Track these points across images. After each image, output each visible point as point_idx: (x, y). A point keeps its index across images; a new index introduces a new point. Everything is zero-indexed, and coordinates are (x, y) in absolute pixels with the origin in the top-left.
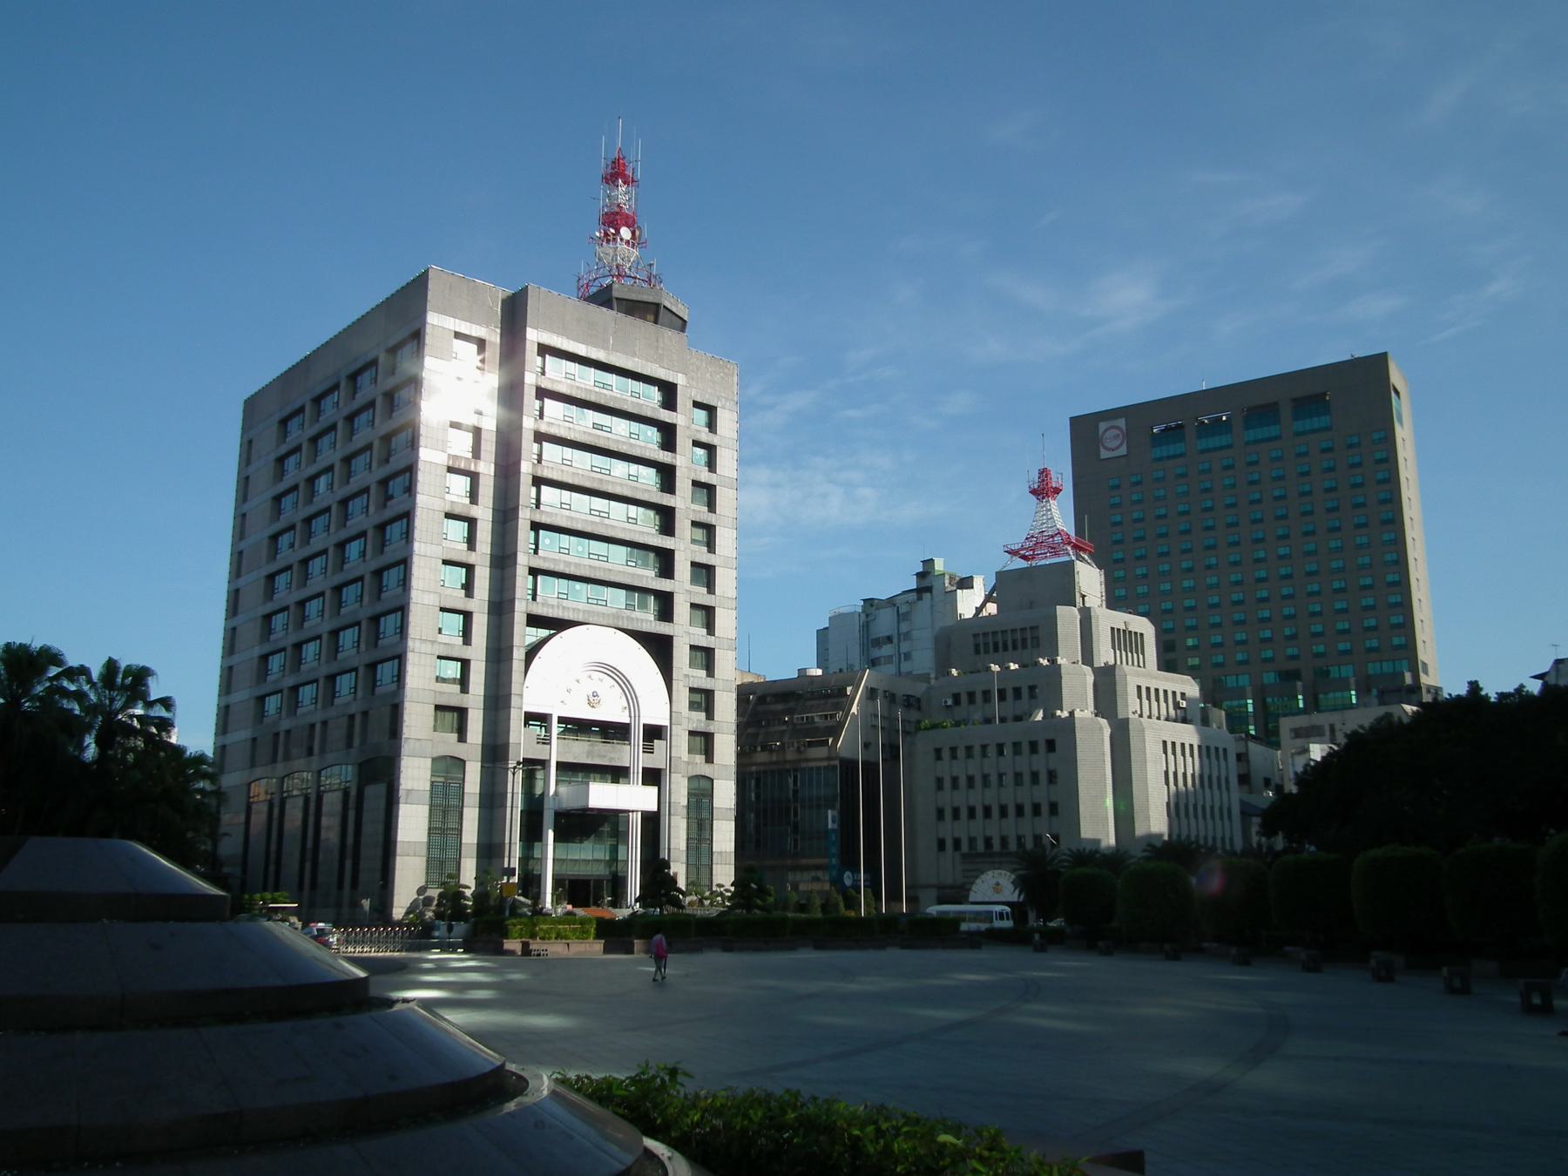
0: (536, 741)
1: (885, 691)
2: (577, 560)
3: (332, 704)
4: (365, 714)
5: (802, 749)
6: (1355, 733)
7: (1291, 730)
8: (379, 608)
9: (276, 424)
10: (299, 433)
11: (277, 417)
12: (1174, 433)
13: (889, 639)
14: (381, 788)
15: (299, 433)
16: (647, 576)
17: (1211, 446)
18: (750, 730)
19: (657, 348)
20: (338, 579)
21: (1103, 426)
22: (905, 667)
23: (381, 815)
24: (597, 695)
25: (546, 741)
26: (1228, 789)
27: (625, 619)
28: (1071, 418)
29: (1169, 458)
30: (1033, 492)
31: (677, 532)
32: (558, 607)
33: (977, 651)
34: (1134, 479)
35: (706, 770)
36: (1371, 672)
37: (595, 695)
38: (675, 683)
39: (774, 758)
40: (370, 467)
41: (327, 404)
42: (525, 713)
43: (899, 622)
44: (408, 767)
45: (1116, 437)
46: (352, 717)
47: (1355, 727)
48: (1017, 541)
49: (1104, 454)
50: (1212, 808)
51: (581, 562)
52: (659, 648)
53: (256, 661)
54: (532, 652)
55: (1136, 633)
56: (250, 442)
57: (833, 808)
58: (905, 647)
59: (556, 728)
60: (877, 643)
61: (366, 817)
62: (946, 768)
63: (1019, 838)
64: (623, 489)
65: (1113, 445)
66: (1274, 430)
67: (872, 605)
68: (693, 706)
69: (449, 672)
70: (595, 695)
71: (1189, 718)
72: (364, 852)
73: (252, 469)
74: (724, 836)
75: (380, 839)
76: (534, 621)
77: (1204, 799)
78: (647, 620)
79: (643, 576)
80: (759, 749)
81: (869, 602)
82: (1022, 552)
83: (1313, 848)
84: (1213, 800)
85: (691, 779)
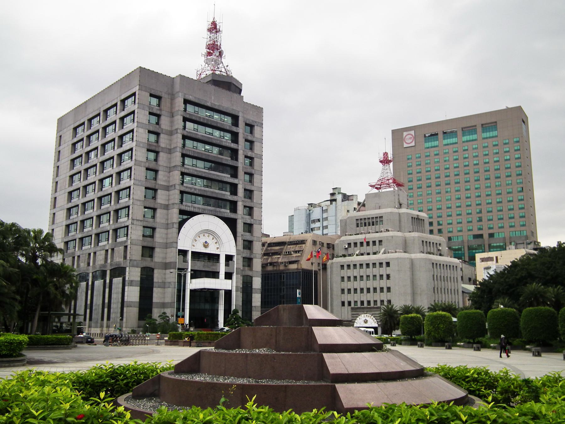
2: (199, 188)
3: (98, 245)
5: (287, 265)
6: (514, 261)
7: (480, 259)
8: (118, 207)
9: (72, 130)
10: (82, 133)
11: (73, 126)
13: (319, 220)
14: (120, 279)
15: (82, 133)
16: (227, 195)
17: (449, 143)
18: (265, 257)
19: (231, 101)
20: (101, 194)
21: (405, 134)
22: (325, 231)
23: (120, 290)
25: (185, 261)
26: (457, 282)
28: (392, 131)
29: (432, 147)
30: (381, 162)
33: (358, 226)
34: (417, 156)
35: (250, 273)
37: (206, 242)
38: (238, 238)
39: (275, 268)
40: (114, 148)
41: (95, 121)
43: (323, 213)
45: (410, 138)
47: (514, 259)
48: (374, 181)
49: (405, 145)
50: (451, 290)
52: (231, 224)
56: (61, 136)
57: (299, 289)
58: (325, 223)
59: (189, 255)
60: (314, 221)
62: (346, 273)
65: (409, 141)
66: (474, 137)
68: (244, 248)
69: (148, 233)
70: (206, 242)
71: (442, 254)
72: (113, 306)
73: (61, 147)
74: (257, 300)
76: (182, 212)
78: (227, 213)
80: (269, 265)
81: (311, 205)
82: (376, 186)
83: (502, 306)
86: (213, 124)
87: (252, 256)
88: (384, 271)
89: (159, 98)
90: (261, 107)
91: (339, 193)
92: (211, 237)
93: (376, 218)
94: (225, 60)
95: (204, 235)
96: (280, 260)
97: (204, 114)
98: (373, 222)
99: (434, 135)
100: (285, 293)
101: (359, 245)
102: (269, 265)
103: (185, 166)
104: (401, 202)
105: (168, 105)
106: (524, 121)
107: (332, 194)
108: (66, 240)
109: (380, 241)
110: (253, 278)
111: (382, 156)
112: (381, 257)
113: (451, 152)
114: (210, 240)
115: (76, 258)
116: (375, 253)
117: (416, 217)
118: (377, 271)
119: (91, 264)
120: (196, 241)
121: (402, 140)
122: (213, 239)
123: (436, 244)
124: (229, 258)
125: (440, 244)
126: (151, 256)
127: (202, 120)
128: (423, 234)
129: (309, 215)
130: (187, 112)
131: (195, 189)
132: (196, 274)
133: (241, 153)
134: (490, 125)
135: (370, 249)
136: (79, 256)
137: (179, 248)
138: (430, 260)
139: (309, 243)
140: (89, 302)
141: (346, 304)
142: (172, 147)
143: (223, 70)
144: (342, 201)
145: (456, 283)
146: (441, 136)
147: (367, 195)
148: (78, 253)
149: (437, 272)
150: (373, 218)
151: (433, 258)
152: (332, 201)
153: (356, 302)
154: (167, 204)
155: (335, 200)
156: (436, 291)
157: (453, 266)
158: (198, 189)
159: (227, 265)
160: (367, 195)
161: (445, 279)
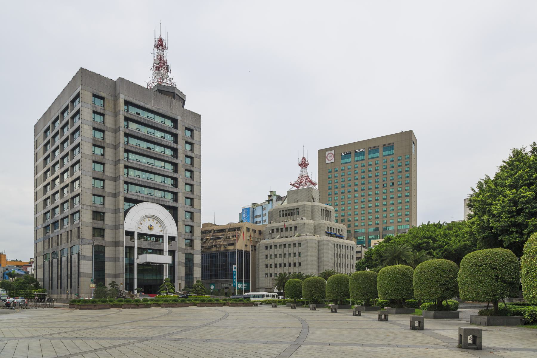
0: (130, 240)
1: (253, 229)
2: (143, 180)
4: (71, 231)
5: (226, 246)
10: (50, 135)
12: (348, 155)
15: (50, 135)
21: (327, 153)
24: (152, 226)
25: (133, 240)
27: (161, 201)
30: (300, 165)
31: (179, 172)
32: (136, 195)
34: (336, 170)
35: (191, 252)
36: (399, 228)
37: (151, 226)
38: (179, 223)
42: (125, 231)
43: (263, 211)
44: (84, 248)
45: (331, 156)
46: (68, 232)
49: (327, 162)
51: (144, 180)
52: (173, 211)
53: (43, 215)
54: (126, 212)
55: (329, 211)
61: (73, 265)
62: (269, 252)
63: (280, 274)
64: (156, 155)
65: (330, 159)
66: (377, 155)
67: (255, 205)
70: (151, 226)
72: (73, 276)
74: (197, 273)
75: (77, 272)
76: (127, 200)
77: (345, 262)
79: (167, 186)
80: (213, 247)
82: (295, 185)
84: (348, 262)
85: (186, 254)
86: (154, 125)
87: (193, 238)
88: (296, 250)
89: (102, 98)
90: (199, 114)
91: (274, 195)
92: (155, 221)
93: (294, 209)
94: (170, 75)
95: (149, 220)
96: (222, 243)
97: (144, 115)
98: (292, 213)
99: (348, 155)
100: (225, 268)
101: (280, 230)
102: (213, 247)
103: (129, 160)
104: (314, 197)
105: (112, 106)
106: (414, 142)
107: (270, 196)
108: (44, 225)
109: (296, 227)
110: (194, 255)
111: (300, 160)
112: (295, 239)
113: (360, 166)
114: (154, 223)
115: (51, 239)
116: (291, 237)
117: (325, 209)
118: (291, 250)
119: (59, 244)
120: (141, 224)
121: (325, 157)
122: (157, 223)
123: (339, 229)
124: (172, 239)
125: (341, 230)
126: (103, 236)
127: (143, 121)
128: (328, 222)
129: (253, 212)
130: (129, 112)
131: (139, 181)
132: (142, 251)
133: (180, 151)
134: (389, 145)
135: (288, 233)
136: (52, 238)
137: (125, 229)
138: (332, 241)
139: (244, 230)
140: (59, 275)
141: (269, 275)
142: (117, 144)
143: (169, 82)
144: (277, 201)
145: (352, 260)
146: (353, 154)
147: (288, 192)
148: (52, 236)
149: (338, 251)
150: (291, 210)
151: (335, 240)
152: (269, 201)
153: (276, 274)
154: (115, 192)
155: (272, 200)
156: (336, 266)
157: (350, 247)
158: (142, 181)
159: (170, 244)
160: (288, 192)
161: (343, 256)
